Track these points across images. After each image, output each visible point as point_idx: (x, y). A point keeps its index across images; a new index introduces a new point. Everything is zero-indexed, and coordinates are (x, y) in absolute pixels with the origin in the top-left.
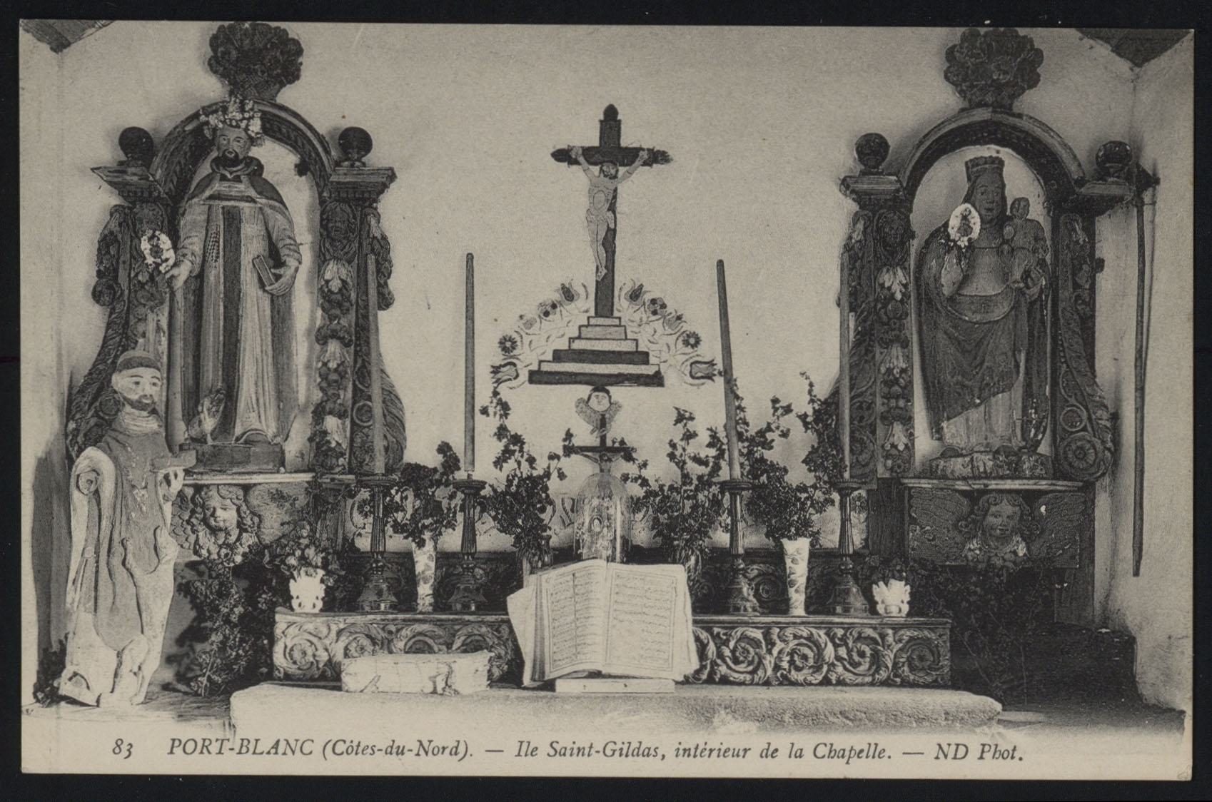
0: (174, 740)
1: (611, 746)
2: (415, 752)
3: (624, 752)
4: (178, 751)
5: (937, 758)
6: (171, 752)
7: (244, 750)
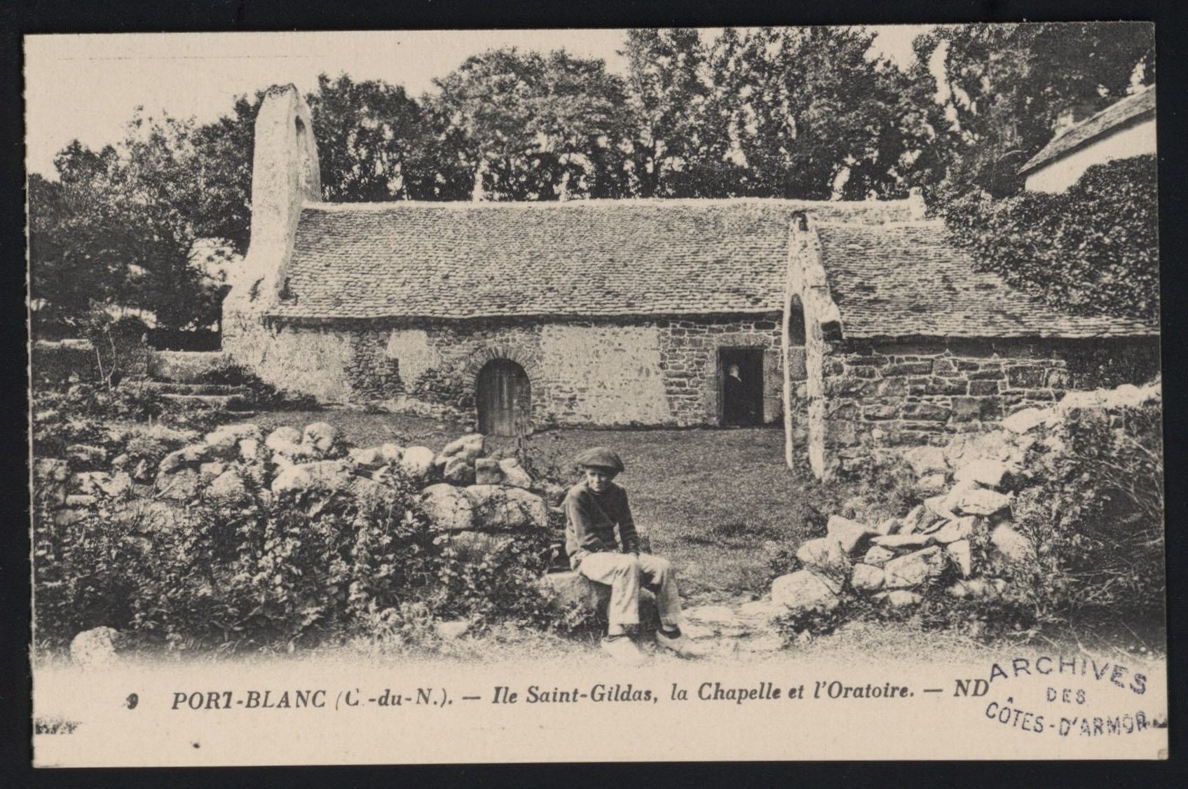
0: (177, 695)
1: (599, 690)
2: (415, 699)
4: (50, 726)
5: (957, 695)
6: (816, 696)
7: (253, 703)
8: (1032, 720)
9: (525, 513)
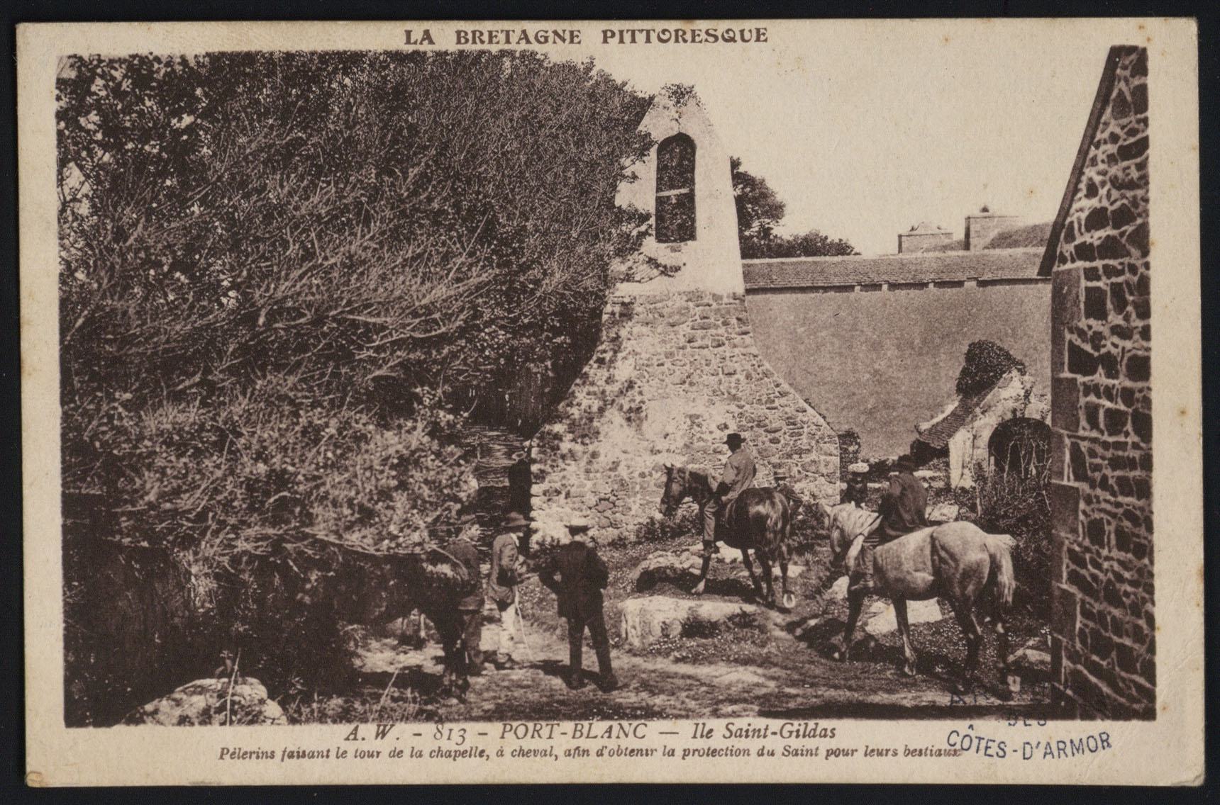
3: (801, 733)
4: (227, 757)
7: (578, 734)
8: (994, 746)
9: (964, 549)
